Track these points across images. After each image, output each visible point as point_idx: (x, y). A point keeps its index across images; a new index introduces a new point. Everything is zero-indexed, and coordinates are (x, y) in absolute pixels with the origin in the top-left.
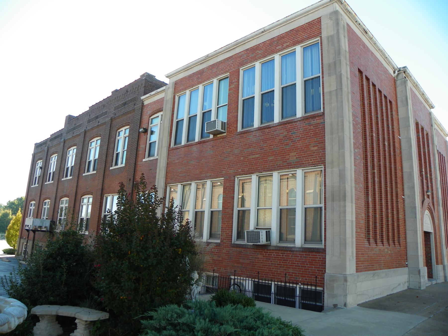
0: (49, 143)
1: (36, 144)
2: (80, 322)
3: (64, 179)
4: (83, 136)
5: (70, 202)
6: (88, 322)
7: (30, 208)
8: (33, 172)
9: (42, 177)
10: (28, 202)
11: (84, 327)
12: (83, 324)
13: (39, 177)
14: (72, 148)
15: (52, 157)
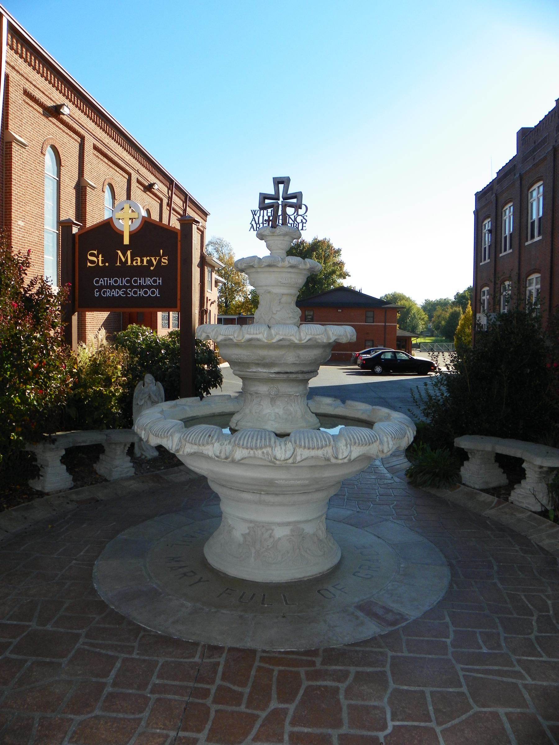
0: (496, 187)
1: (477, 194)
2: (529, 468)
3: (529, 242)
4: (552, 158)
5: (543, 279)
6: (545, 469)
7: (483, 298)
8: (480, 240)
9: (493, 246)
10: (479, 288)
11: (537, 476)
12: (536, 472)
13: (489, 246)
14: (535, 186)
15: (504, 209)
